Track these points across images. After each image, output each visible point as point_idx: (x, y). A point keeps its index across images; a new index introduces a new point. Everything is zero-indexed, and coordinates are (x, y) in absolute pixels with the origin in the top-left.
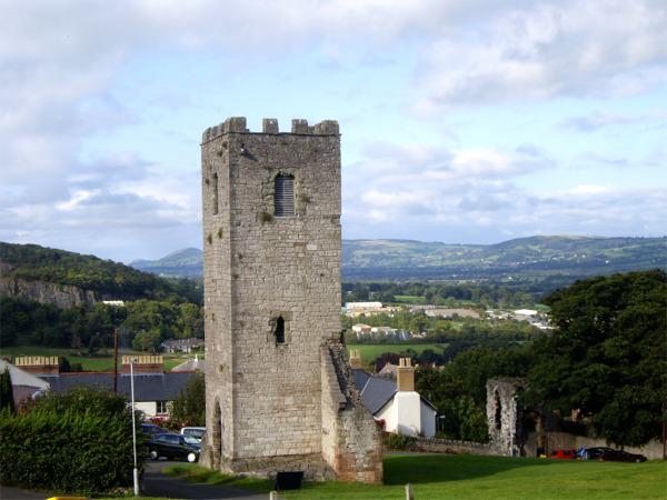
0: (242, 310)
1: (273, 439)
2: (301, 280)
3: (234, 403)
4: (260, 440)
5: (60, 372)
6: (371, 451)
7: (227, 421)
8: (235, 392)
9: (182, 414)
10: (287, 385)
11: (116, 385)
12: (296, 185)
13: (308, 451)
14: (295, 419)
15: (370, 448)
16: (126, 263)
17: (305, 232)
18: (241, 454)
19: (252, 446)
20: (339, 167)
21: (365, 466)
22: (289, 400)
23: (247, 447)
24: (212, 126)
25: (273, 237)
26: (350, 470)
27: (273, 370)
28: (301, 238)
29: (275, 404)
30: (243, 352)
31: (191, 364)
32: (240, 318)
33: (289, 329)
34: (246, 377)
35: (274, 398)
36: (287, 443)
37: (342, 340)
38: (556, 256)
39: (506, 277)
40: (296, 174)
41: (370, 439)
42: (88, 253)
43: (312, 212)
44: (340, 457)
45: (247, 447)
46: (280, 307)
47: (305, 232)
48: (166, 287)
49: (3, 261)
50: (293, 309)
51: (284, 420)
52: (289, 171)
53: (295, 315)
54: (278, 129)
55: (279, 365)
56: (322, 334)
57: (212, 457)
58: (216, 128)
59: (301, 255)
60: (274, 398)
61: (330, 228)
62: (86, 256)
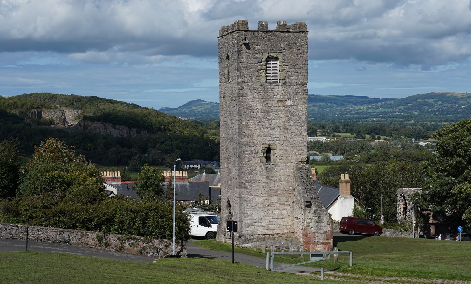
1: (263, 224)
5: (121, 181)
6: (326, 232)
8: (240, 194)
11: (210, 194)
13: (286, 231)
14: (278, 211)
16: (157, 109)
17: (284, 93)
19: (250, 228)
22: (274, 199)
23: (247, 229)
24: (225, 25)
31: (200, 179)
36: (272, 227)
37: (307, 162)
38: (444, 107)
39: (410, 120)
40: (280, 56)
44: (305, 235)
46: (269, 141)
47: (284, 93)
49: (307, 89)
51: (270, 212)
52: (274, 55)
54: (268, 28)
56: (295, 158)
58: (228, 27)
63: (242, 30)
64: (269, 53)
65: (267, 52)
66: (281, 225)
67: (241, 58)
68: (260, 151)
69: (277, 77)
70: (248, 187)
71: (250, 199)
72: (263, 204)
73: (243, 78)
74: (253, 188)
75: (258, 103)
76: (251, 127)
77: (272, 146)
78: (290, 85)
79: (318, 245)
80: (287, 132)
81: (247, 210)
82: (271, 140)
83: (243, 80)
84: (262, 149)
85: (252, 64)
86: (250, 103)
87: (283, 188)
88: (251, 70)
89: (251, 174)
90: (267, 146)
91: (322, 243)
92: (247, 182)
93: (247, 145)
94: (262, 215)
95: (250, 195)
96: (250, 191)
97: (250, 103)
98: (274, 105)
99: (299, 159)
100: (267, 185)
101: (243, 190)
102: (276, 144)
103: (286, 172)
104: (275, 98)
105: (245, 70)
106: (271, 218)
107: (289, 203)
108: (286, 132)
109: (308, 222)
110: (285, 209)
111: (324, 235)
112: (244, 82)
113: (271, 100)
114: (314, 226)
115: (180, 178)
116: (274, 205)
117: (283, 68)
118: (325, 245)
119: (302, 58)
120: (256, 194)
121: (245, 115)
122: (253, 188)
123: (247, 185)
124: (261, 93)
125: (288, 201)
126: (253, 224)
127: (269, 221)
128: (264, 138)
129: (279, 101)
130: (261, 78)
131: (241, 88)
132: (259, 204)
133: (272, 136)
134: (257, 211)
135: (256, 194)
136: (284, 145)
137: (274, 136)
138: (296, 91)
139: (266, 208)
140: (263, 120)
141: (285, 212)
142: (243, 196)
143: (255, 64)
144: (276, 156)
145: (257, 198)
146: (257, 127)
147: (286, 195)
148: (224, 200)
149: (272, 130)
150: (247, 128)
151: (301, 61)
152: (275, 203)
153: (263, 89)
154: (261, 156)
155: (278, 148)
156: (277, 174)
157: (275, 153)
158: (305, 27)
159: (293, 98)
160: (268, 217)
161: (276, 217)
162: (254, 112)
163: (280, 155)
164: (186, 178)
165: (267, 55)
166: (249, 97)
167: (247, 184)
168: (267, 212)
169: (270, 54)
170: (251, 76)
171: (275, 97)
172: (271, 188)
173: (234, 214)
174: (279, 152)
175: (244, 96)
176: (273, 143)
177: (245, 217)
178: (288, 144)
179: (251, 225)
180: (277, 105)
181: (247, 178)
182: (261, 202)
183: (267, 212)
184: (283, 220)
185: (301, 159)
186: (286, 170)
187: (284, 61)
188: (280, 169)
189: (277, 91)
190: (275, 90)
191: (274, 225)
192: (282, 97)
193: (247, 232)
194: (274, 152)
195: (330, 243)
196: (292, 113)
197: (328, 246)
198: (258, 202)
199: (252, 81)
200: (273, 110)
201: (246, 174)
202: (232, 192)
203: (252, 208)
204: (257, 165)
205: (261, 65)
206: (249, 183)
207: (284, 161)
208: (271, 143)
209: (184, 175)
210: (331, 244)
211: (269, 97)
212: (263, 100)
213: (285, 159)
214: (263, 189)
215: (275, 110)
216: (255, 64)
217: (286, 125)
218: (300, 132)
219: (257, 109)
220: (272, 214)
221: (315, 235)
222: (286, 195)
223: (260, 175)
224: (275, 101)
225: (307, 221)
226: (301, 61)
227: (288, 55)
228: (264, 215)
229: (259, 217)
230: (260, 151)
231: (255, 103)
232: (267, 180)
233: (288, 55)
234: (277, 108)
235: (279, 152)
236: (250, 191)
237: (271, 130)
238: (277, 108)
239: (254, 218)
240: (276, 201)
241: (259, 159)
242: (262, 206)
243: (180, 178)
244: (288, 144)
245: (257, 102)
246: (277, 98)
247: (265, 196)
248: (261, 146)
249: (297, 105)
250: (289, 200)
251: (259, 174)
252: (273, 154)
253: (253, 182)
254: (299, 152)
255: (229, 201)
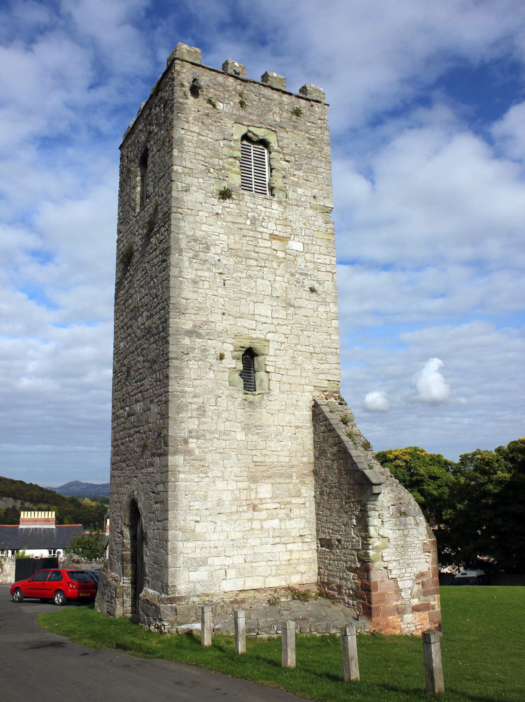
1: (238, 560)
4: (217, 561)
6: (422, 575)
7: (277, 469)
9: (126, 625)
17: (286, 222)
21: (415, 602)
23: (194, 576)
25: (240, 220)
28: (279, 230)
36: (262, 567)
42: (19, 480)
45: (194, 576)
50: (269, 336)
51: (256, 525)
53: (272, 346)
55: (247, 428)
59: (281, 254)
60: (241, 485)
62: (17, 481)
63: (187, 62)
64: (248, 126)
69: (256, 187)
70: (197, 452)
71: (202, 488)
72: (236, 502)
73: (188, 165)
75: (222, 231)
78: (296, 206)
82: (254, 327)
83: (186, 170)
85: (209, 140)
86: (204, 227)
88: (209, 152)
89: (202, 410)
91: (416, 609)
92: (192, 437)
93: (190, 333)
94: (233, 536)
95: (201, 475)
96: (202, 463)
97: (204, 227)
98: (261, 243)
99: (322, 385)
102: (267, 341)
105: (192, 150)
107: (302, 501)
109: (377, 546)
114: (394, 558)
116: (264, 506)
118: (421, 613)
125: (299, 495)
126: (210, 561)
131: (182, 187)
133: (257, 317)
134: (219, 524)
137: (264, 320)
141: (294, 526)
143: (217, 140)
145: (220, 485)
147: (295, 478)
150: (195, 289)
152: (268, 500)
154: (229, 366)
159: (303, 234)
161: (271, 541)
166: (201, 213)
167: (193, 444)
168: (248, 525)
169: (251, 129)
170: (207, 164)
172: (255, 459)
173: (150, 535)
177: (187, 540)
179: (204, 562)
181: (193, 424)
182: (230, 498)
183: (248, 525)
184: (289, 547)
190: (264, 209)
192: (279, 228)
195: (433, 608)
196: (302, 269)
197: (430, 615)
198: (224, 498)
199: (210, 177)
201: (189, 415)
203: (208, 512)
204: (222, 391)
216: (217, 140)
217: (292, 296)
220: (259, 532)
222: (295, 478)
230: (228, 355)
234: (268, 251)
236: (202, 463)
239: (212, 544)
242: (234, 509)
245: (221, 228)
246: (267, 228)
247: (240, 479)
250: (302, 491)
251: (225, 415)
253: (208, 436)
254: (322, 366)
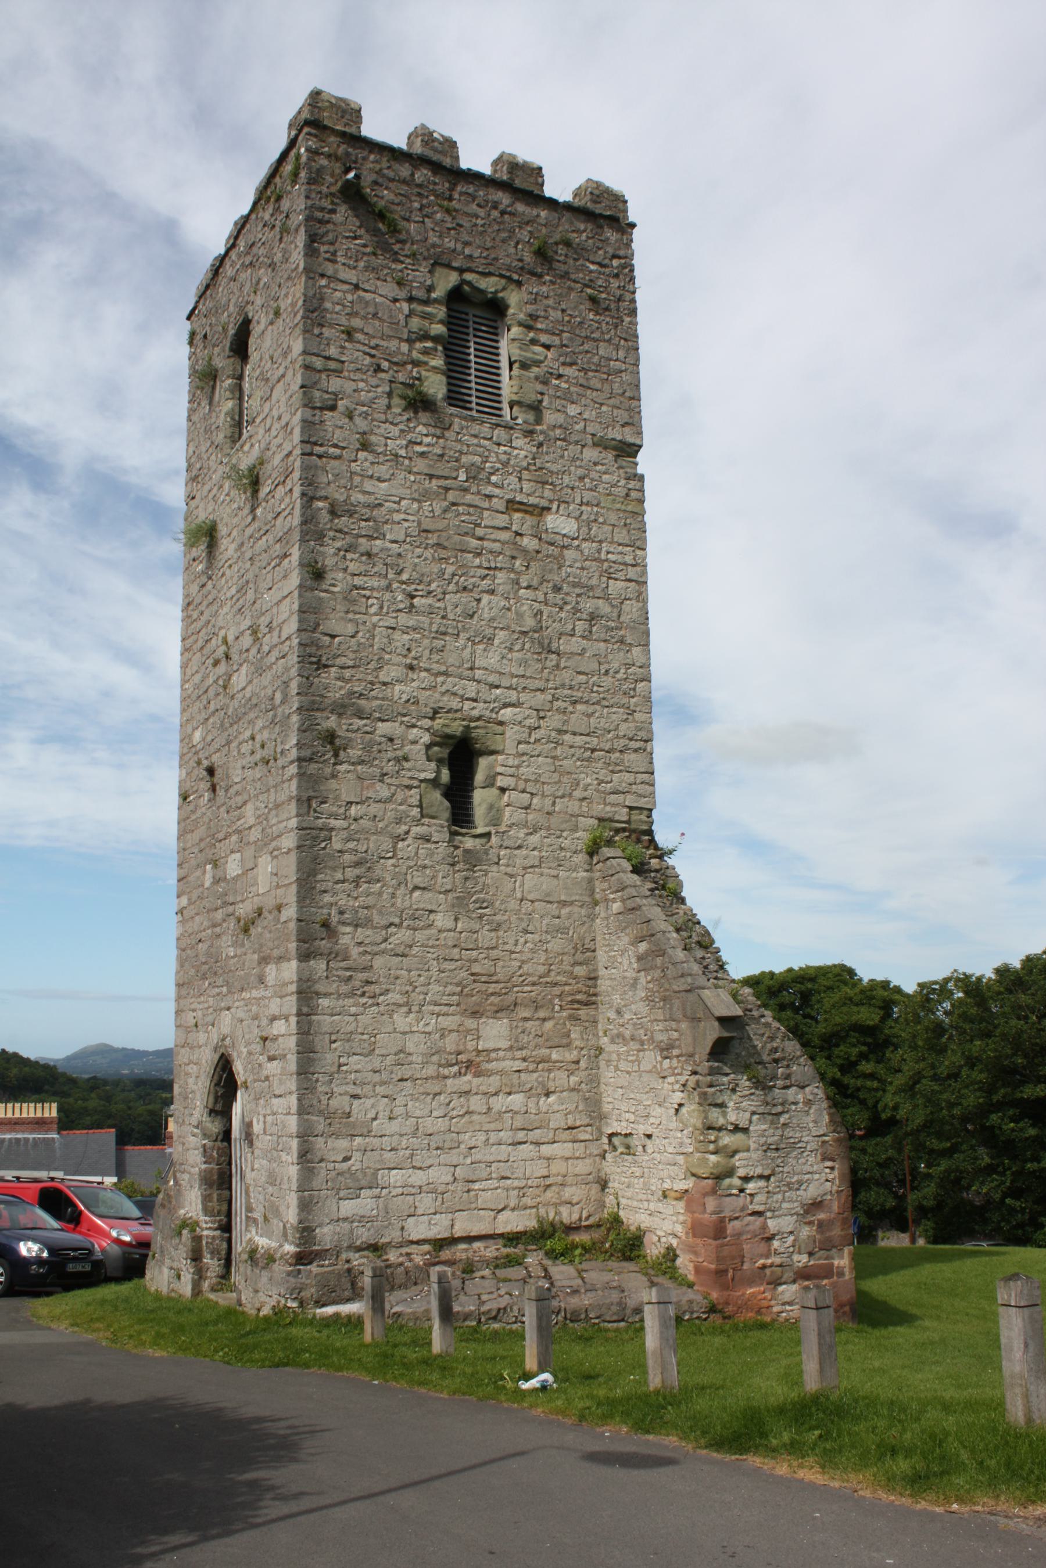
0: (337, 692)
1: (440, 1175)
2: (530, 622)
3: (307, 1051)
6: (816, 1205)
10: (490, 978)
12: (506, 347)
14: (516, 1100)
15: (811, 1192)
16: (33, 1058)
18: (326, 1235)
19: (364, 1204)
20: (633, 312)
21: (801, 1260)
23: (348, 1208)
25: (441, 469)
26: (751, 1282)
27: (441, 920)
28: (529, 493)
29: (450, 1043)
30: (337, 844)
32: (331, 722)
33: (490, 783)
34: (347, 937)
35: (446, 1022)
41: (812, 1162)
43: (560, 418)
45: (348, 1208)
48: (105, 1082)
51: (476, 1103)
52: (489, 285)
53: (512, 733)
56: (599, 809)
57: (196, 1257)
60: (446, 1022)
61: (613, 476)
65: (455, 264)
66: (536, 1182)
67: (327, 256)
68: (417, 751)
70: (355, 952)
74: (378, 962)
76: (373, 610)
77: (481, 731)
78: (564, 440)
79: (781, 1288)
80: (557, 666)
81: (346, 1093)
82: (473, 695)
84: (426, 738)
85: (378, 299)
87: (542, 969)
90: (456, 728)
92: (344, 924)
94: (429, 1124)
95: (364, 1000)
99: (617, 817)
100: (456, 950)
101: (324, 966)
102: (501, 723)
103: (555, 882)
104: (495, 485)
106: (479, 1144)
107: (573, 1055)
108: (549, 664)
110: (551, 1085)
111: (810, 1223)
112: (338, 372)
113: (474, 489)
114: (759, 1171)
115: (37, 1123)
116: (493, 1065)
117: (529, 355)
119: (613, 332)
120: (394, 997)
121: (338, 544)
122: (378, 962)
123: (345, 940)
124: (425, 449)
127: (469, 1161)
128: (440, 679)
129: (513, 506)
130: (424, 373)
132: (414, 1058)
133: (478, 673)
135: (394, 997)
136: (542, 731)
137: (492, 678)
138: (593, 475)
139: (449, 1081)
140: (433, 586)
141: (556, 1107)
142: (324, 1002)
144: (503, 790)
145: (401, 1021)
146: (404, 619)
148: (193, 1069)
149: (481, 647)
151: (609, 341)
153: (432, 430)
154: (422, 776)
155: (510, 746)
156: (510, 886)
157: (499, 769)
158: (621, 205)
160: (462, 1137)
162: (388, 537)
163: (521, 785)
164: (51, 1123)
165: (453, 278)
169: (468, 276)
170: (373, 352)
171: (494, 478)
172: (477, 968)
174: (518, 767)
175: (336, 446)
176: (487, 713)
178: (560, 732)
180: (501, 520)
184: (545, 1149)
185: (625, 818)
186: (554, 872)
187: (531, 323)
188: (528, 862)
189: (505, 453)
191: (494, 1183)
192: (526, 486)
193: (346, 1226)
194: (491, 767)
198: (410, 1047)
200: (486, 544)
202: (248, 1003)
203: (376, 1078)
205: (426, 316)
206: (357, 926)
207: (542, 820)
208: (475, 713)
209: (46, 1115)
210: (847, 1276)
211: (462, 477)
212: (434, 482)
213: (550, 809)
214: (434, 972)
215: (496, 546)
218: (618, 676)
219: (406, 524)
221: (765, 1227)
223: (416, 888)
224: (495, 500)
225: (721, 1143)
226: (609, 341)
227: (551, 302)
228: (442, 1124)
229: (414, 1134)
231: (394, 492)
232: (456, 920)
233: (551, 302)
235: (518, 767)
237: (474, 643)
238: (505, 536)
240: (505, 1044)
241: (414, 796)
242: (431, 1071)
243: (37, 1123)
244: (560, 732)
246: (502, 487)
247: (445, 1009)
248: (426, 723)
249: (601, 542)
250: (573, 1036)
252: (488, 777)
255: (224, 1069)
